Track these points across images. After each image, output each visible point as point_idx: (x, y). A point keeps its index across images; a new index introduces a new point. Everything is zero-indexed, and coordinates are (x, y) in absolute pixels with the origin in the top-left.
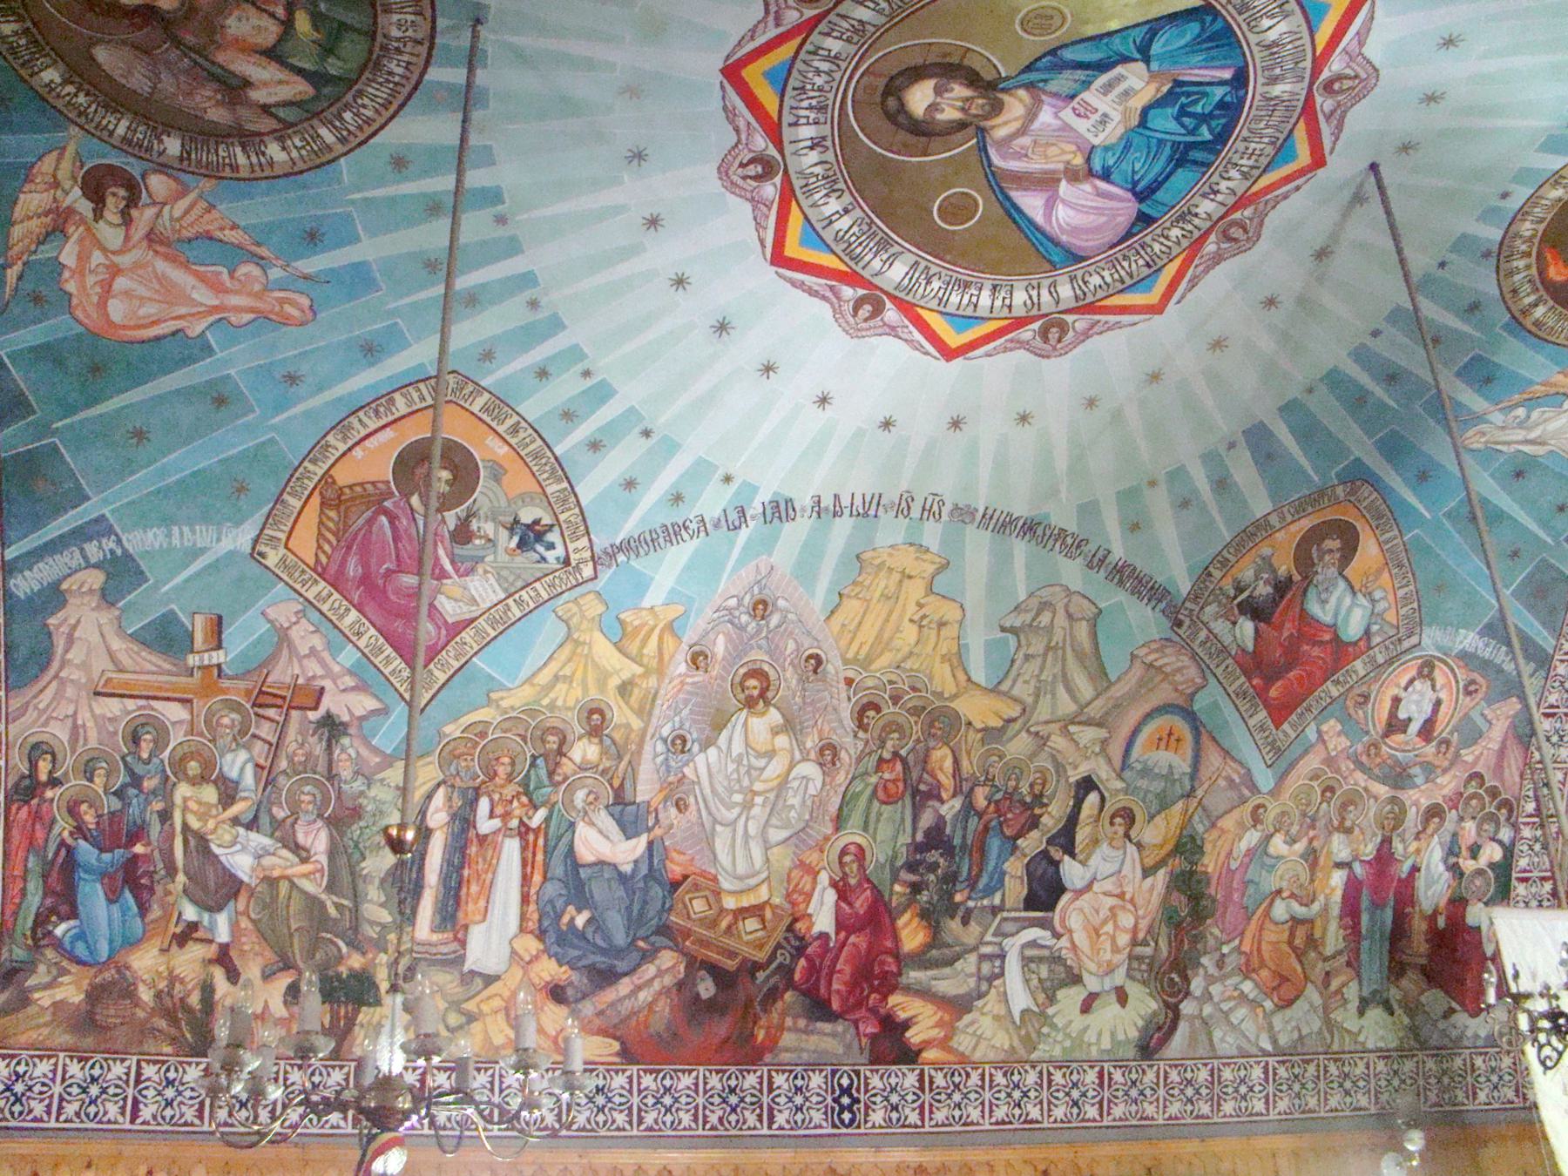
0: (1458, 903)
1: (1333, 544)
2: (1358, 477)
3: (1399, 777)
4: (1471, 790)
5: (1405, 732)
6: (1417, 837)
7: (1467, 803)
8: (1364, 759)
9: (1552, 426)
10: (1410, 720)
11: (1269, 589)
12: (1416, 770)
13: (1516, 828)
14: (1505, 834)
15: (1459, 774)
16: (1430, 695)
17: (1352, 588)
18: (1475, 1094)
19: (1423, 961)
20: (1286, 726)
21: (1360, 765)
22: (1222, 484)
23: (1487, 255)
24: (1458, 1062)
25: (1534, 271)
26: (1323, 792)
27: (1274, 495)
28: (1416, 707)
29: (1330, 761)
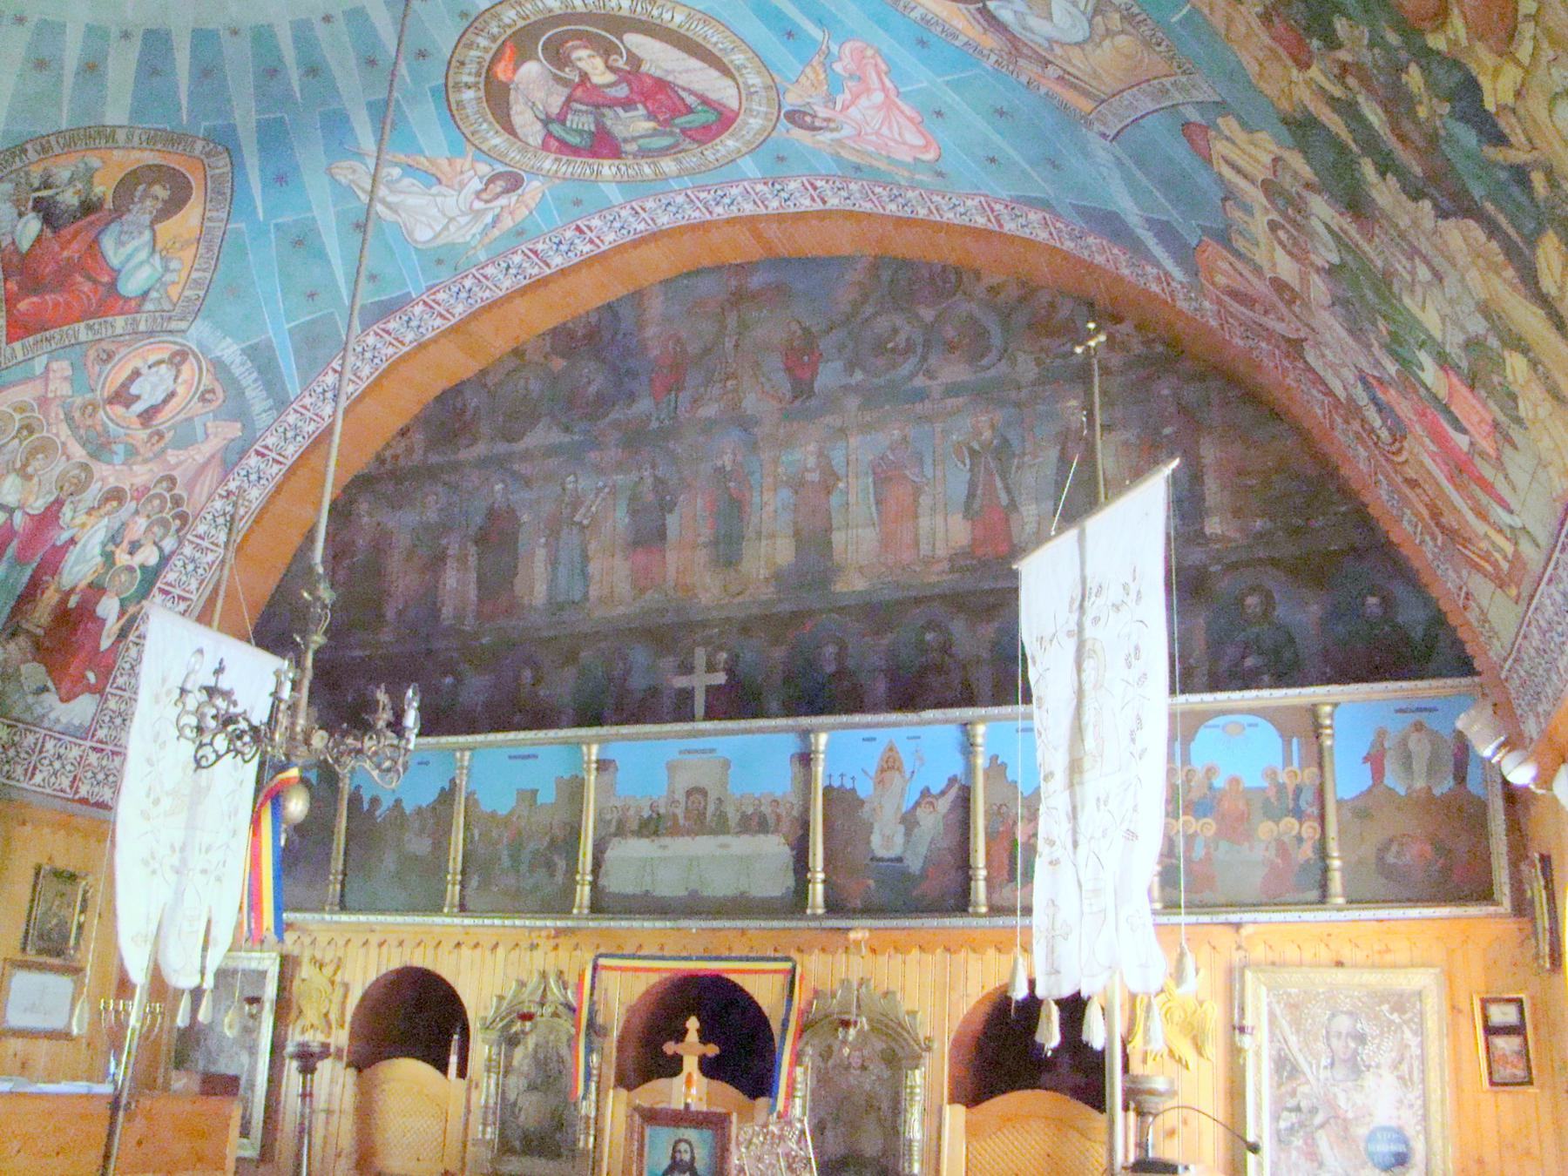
0: (96, 590)
1: (161, 192)
2: (225, 142)
3: (100, 447)
4: (158, 490)
5: (127, 406)
6: (90, 512)
7: (150, 500)
8: (77, 415)
9: (411, 201)
10: (138, 397)
11: (75, 201)
12: (119, 448)
13: (180, 543)
14: (169, 544)
15: (158, 470)
16: (169, 385)
17: (154, 246)
18: (33, 774)
19: (40, 632)
20: (17, 345)
21: (69, 418)
22: (92, 68)
23: (464, 15)
24: (31, 739)
25: (488, 57)
26: (21, 428)
27: (137, 112)
28: (148, 390)
29: (43, 402)
